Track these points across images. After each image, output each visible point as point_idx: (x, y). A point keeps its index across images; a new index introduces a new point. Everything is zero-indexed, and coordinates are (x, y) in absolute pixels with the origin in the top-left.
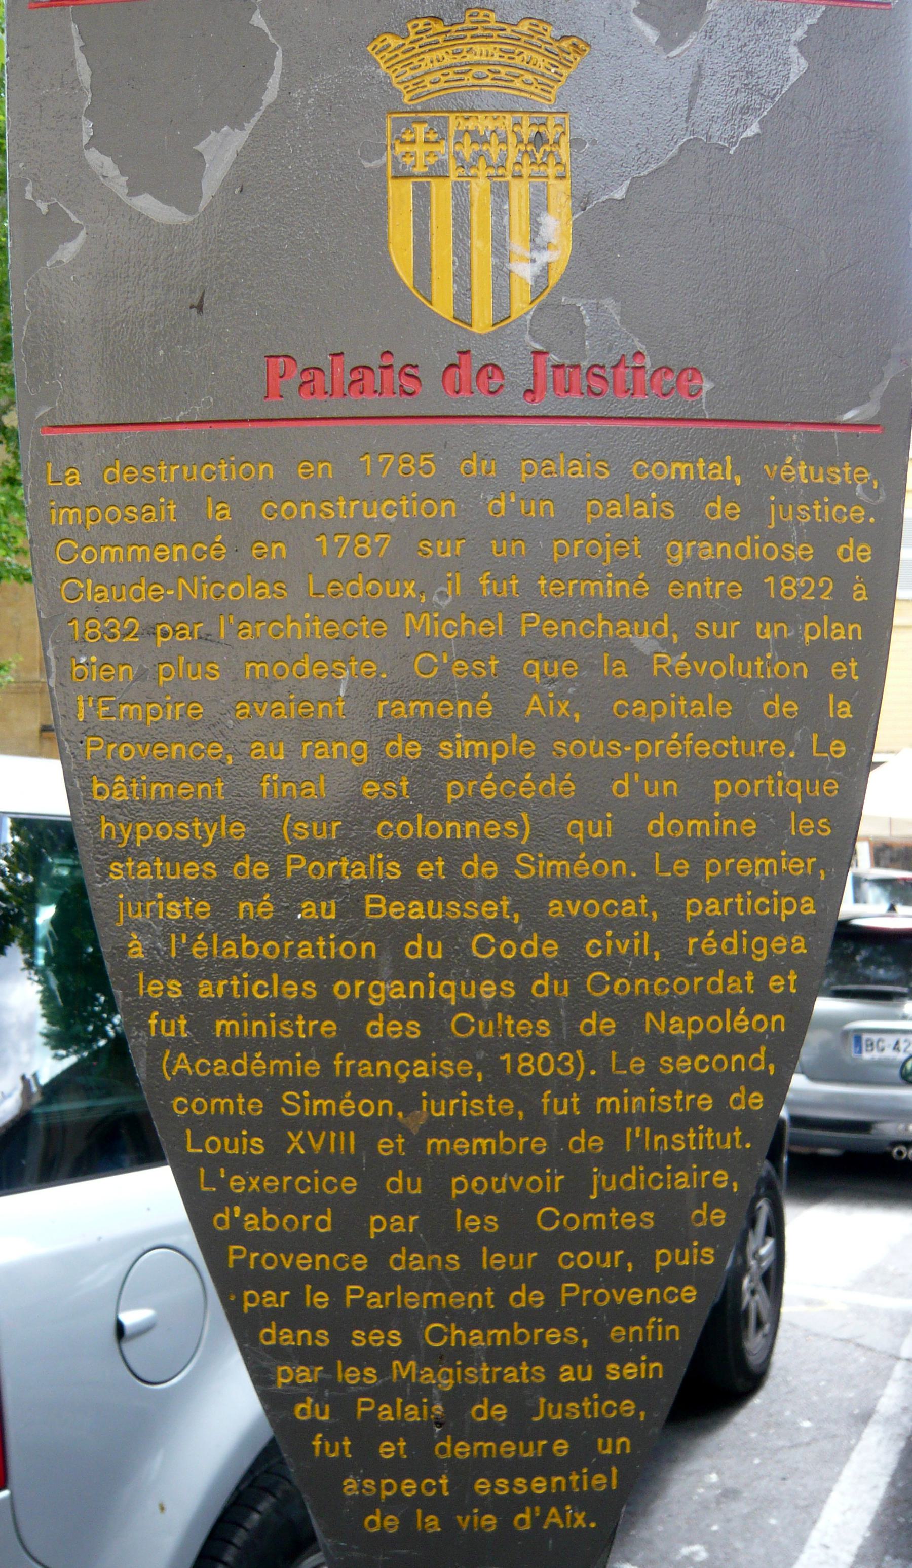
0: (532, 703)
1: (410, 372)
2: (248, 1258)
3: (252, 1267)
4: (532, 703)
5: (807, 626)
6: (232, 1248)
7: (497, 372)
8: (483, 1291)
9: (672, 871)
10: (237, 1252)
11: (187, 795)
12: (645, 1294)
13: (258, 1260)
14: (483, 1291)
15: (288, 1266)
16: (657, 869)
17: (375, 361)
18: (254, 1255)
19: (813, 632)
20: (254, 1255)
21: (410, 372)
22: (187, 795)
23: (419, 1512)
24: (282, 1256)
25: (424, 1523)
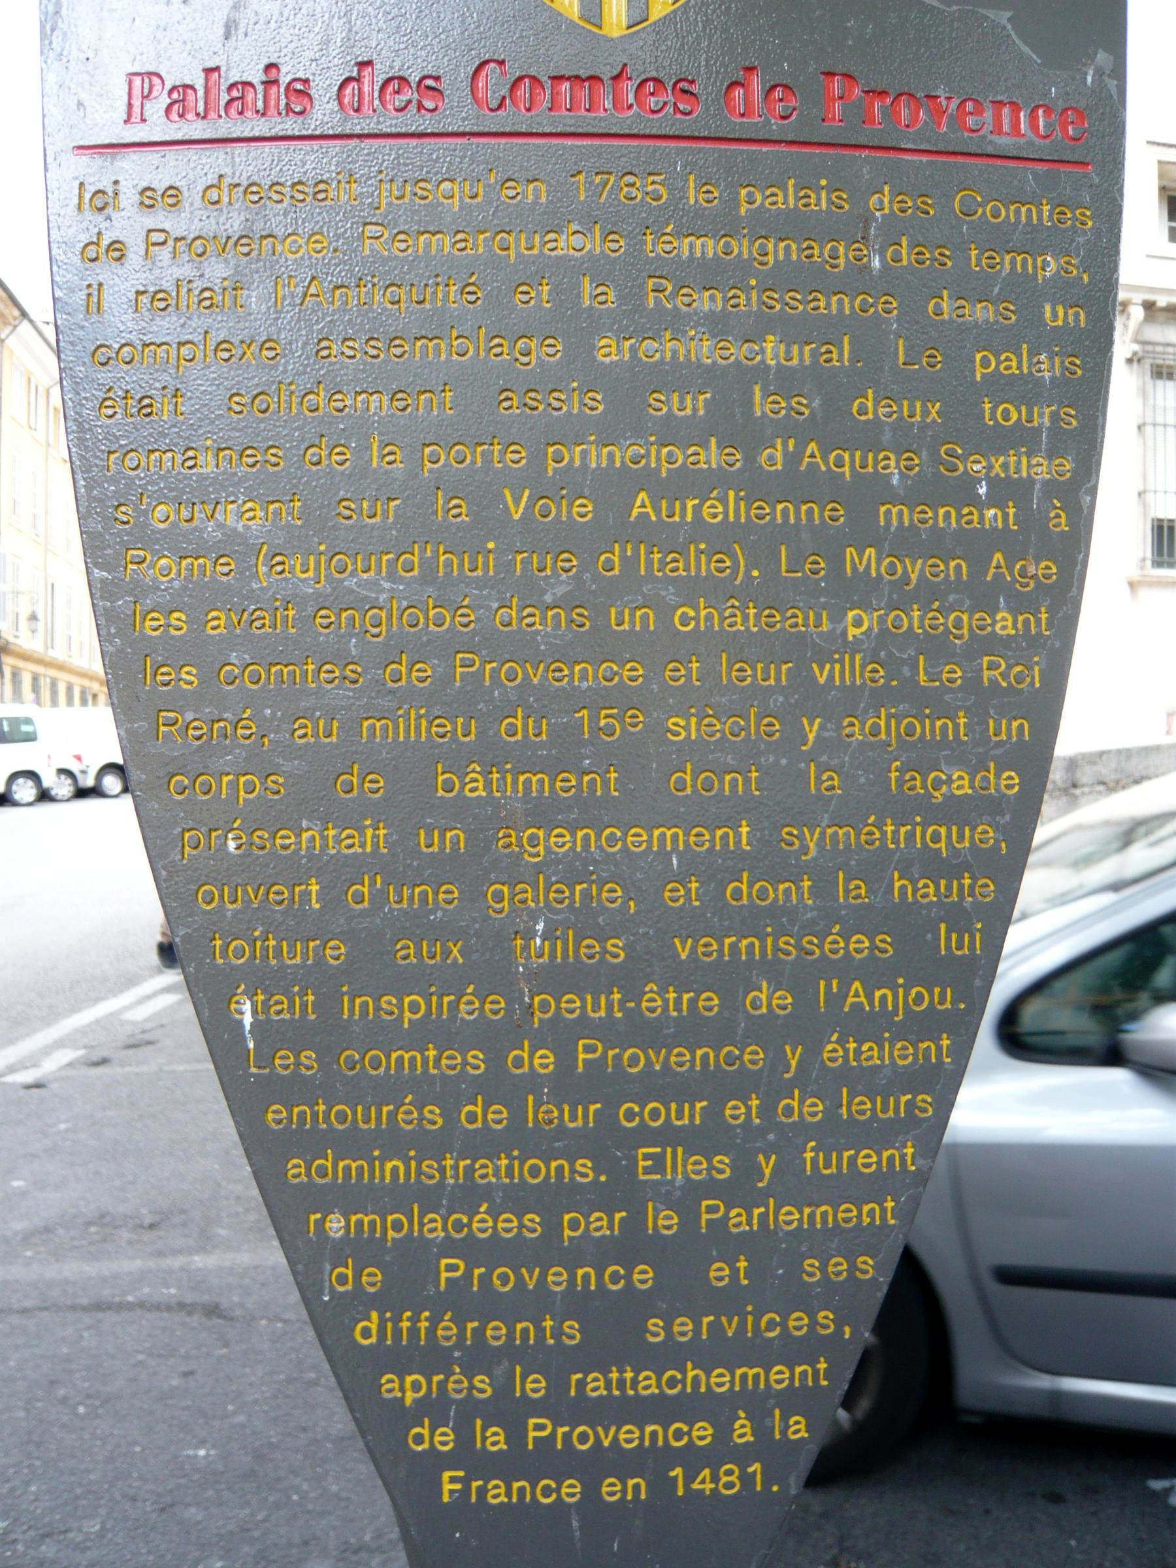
0: (638, 503)
1: (300, 91)
2: (553, 1434)
3: (559, 1447)
4: (638, 503)
5: (978, 357)
6: (532, 1421)
7: (404, 84)
8: (813, 1363)
9: (804, 571)
10: (539, 1427)
11: (377, 791)
12: (651, 836)
13: (567, 1437)
14: (813, 1363)
15: (606, 1443)
16: (784, 568)
17: (256, 76)
18: (561, 1431)
19: (985, 363)
20: (561, 1431)
21: (300, 91)
22: (377, 791)
23: (479, 1422)
24: (600, 1429)
25: (484, 1439)
